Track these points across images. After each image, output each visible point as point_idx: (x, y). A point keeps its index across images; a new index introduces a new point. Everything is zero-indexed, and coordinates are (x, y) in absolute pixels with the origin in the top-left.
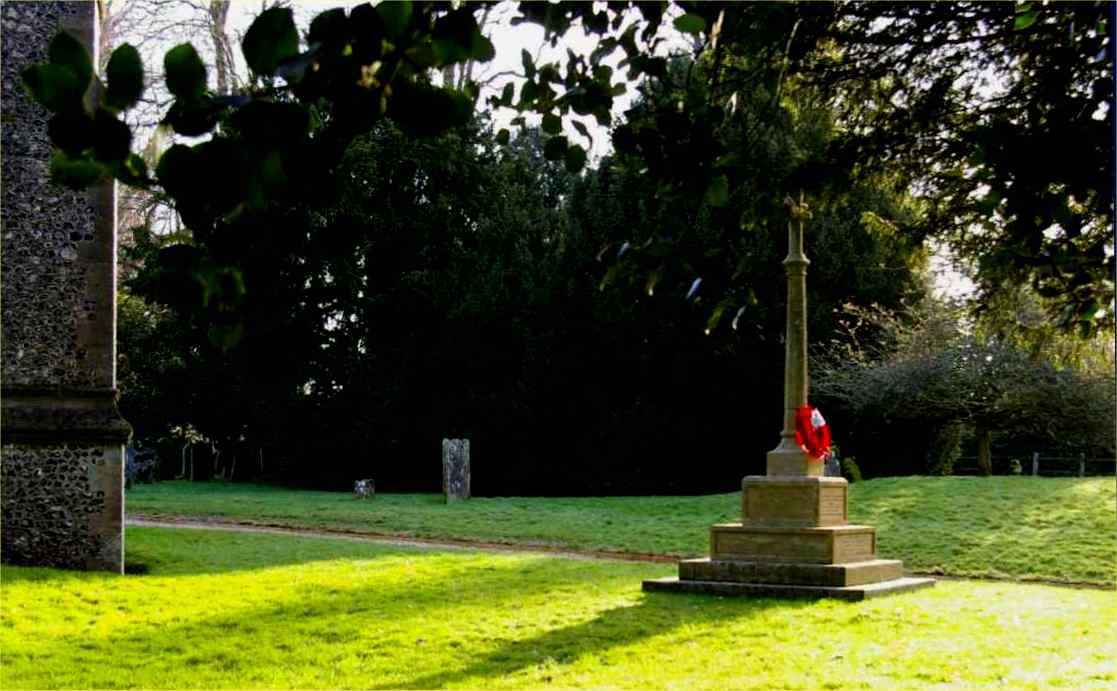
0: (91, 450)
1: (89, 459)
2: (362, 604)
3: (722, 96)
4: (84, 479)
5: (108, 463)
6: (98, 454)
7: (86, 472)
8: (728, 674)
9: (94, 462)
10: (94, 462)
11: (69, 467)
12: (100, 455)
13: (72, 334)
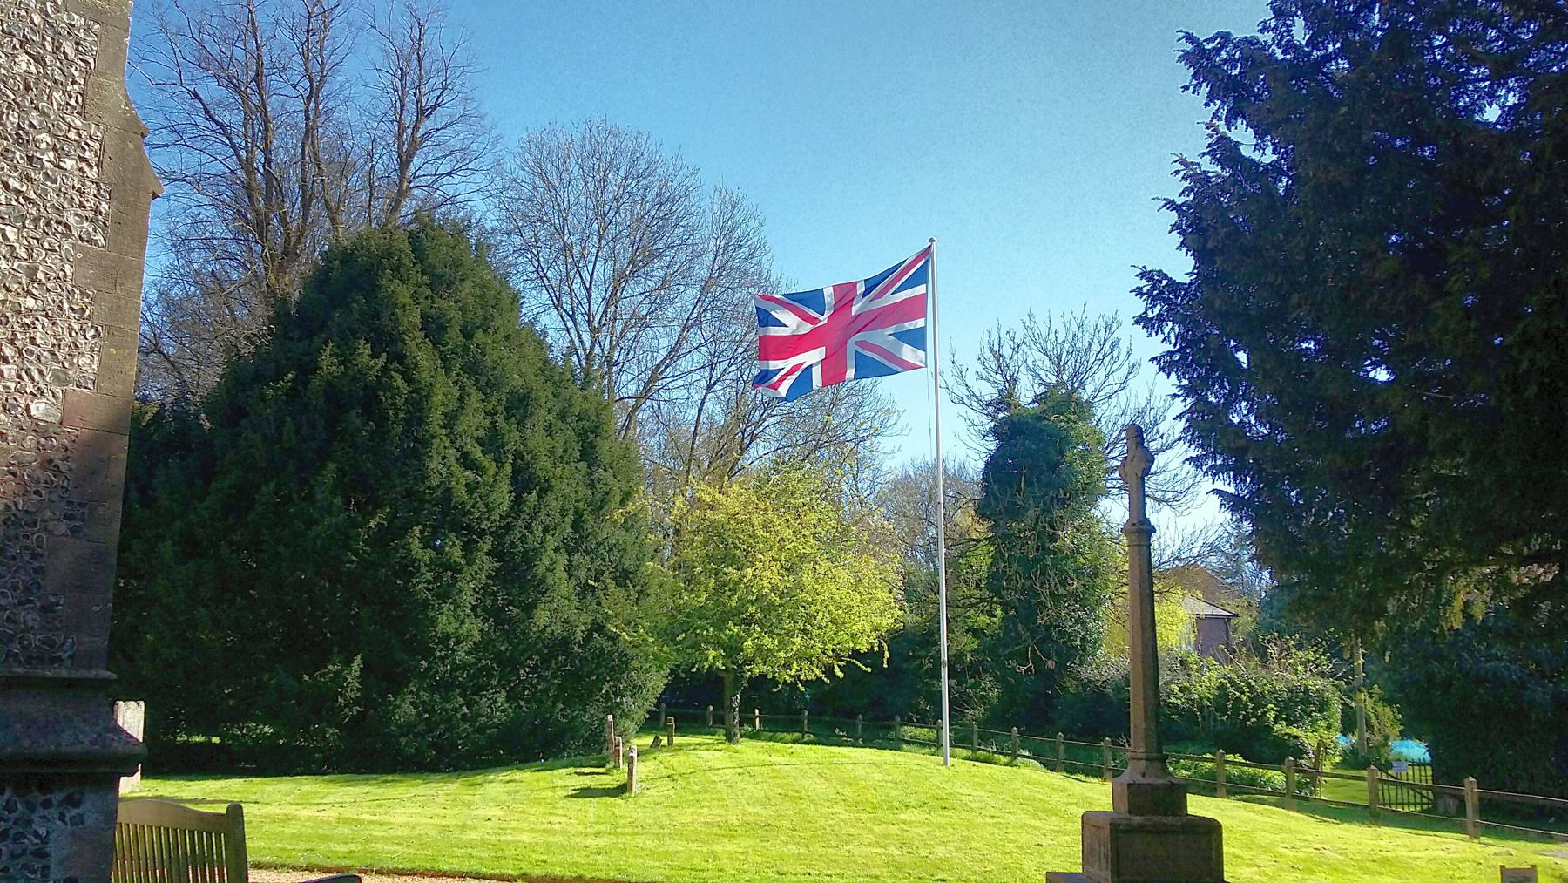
0: (57, 797)
1: (53, 812)
2: (594, 773)
3: (1492, 135)
4: (41, 854)
5: (90, 821)
6: (73, 802)
7: (44, 840)
8: (859, 581)
9: (62, 818)
10: (62, 818)
11: (12, 832)
12: (77, 804)
13: (36, 564)
